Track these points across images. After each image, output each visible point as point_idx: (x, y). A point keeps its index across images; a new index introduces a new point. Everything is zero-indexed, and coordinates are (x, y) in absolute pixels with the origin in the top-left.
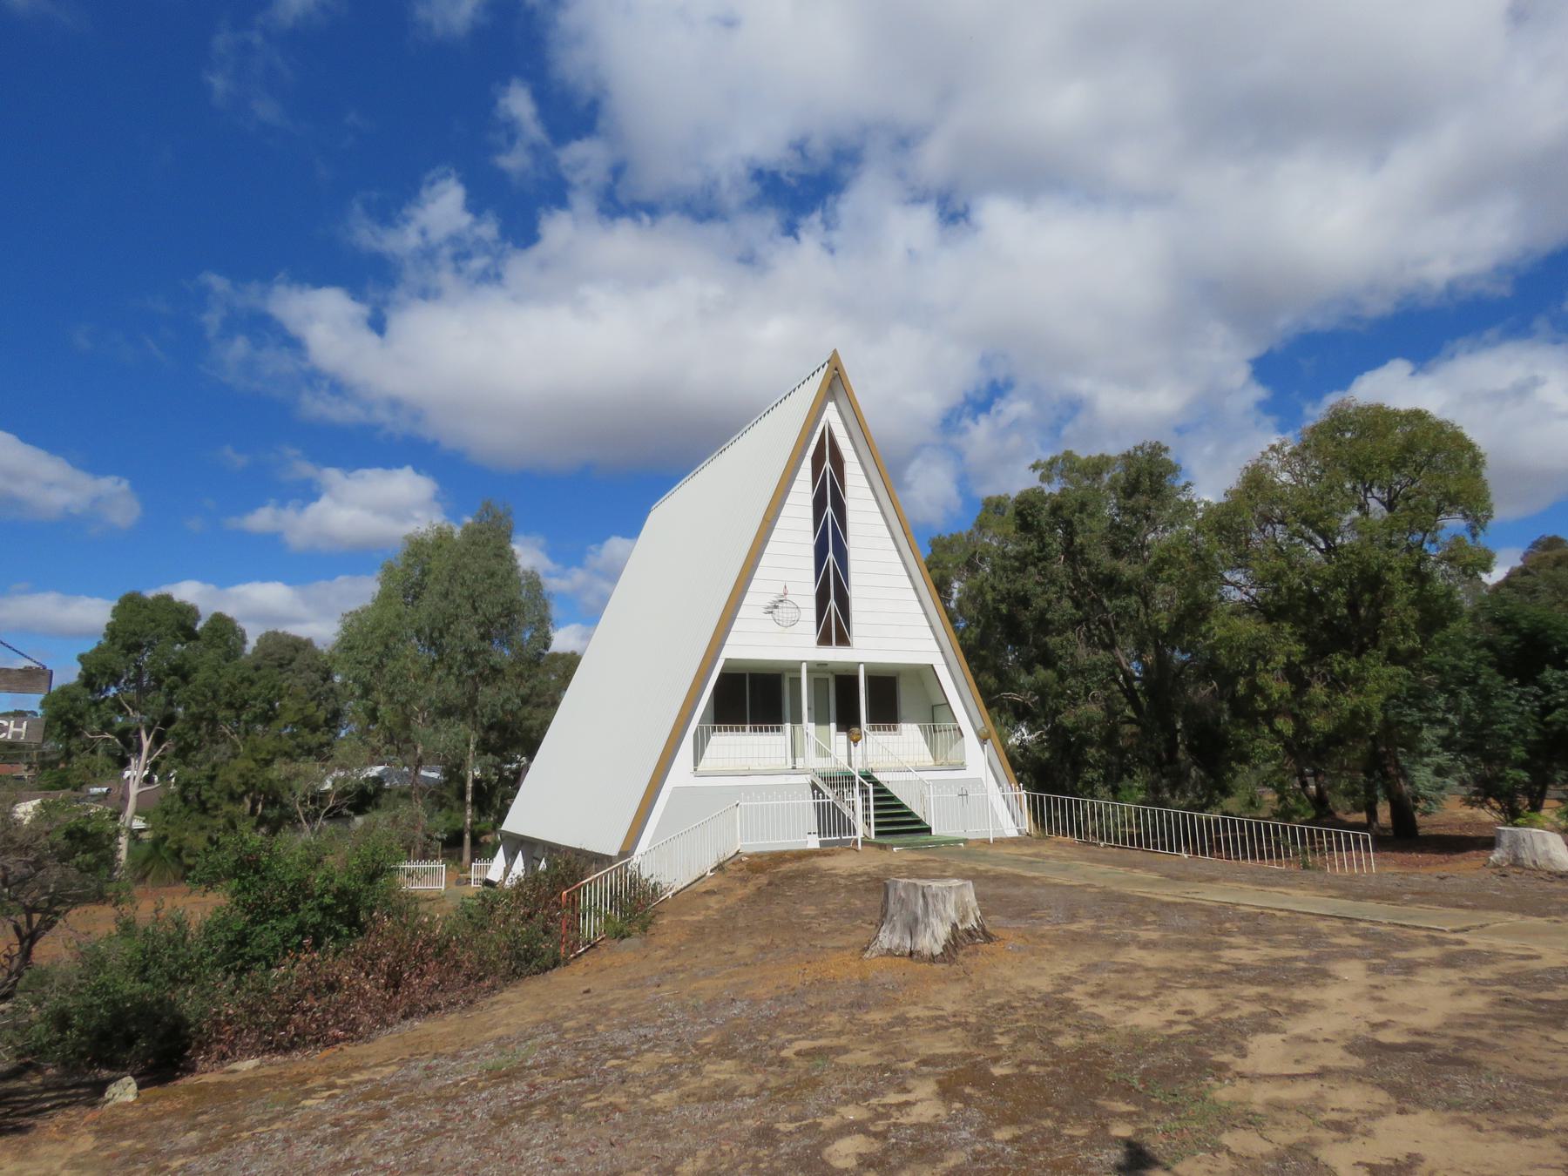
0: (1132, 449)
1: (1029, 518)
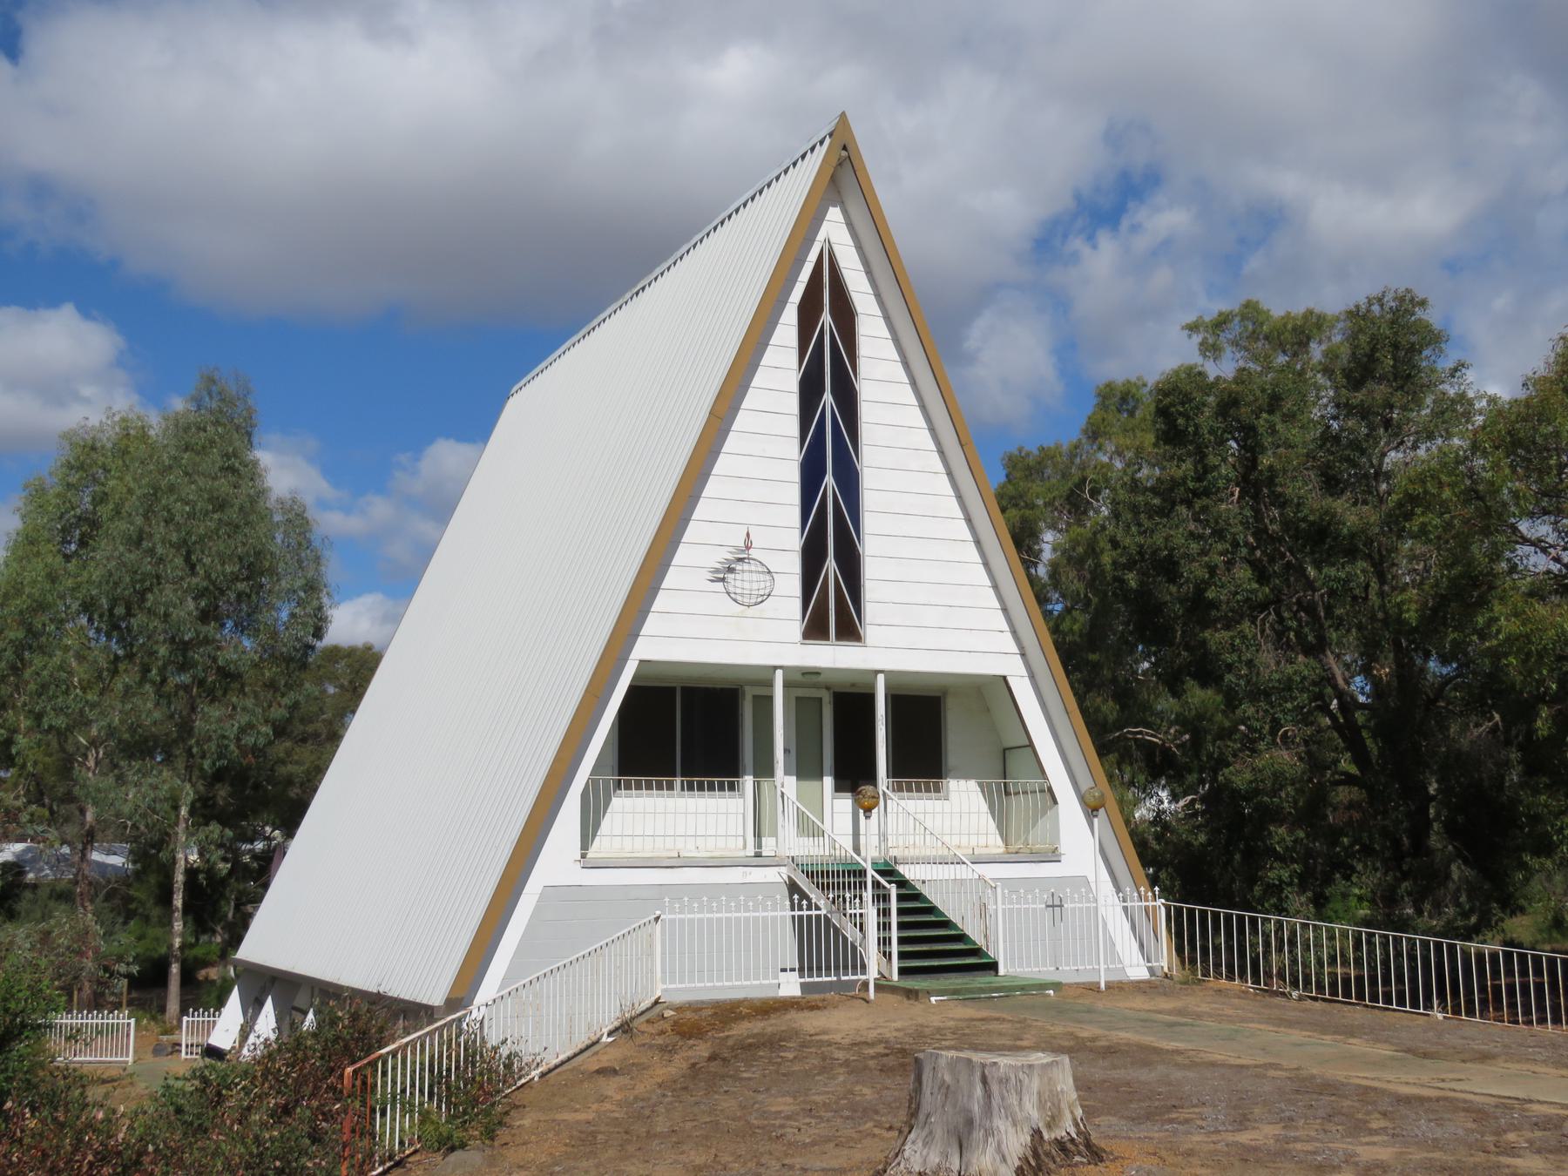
1: (1181, 421)
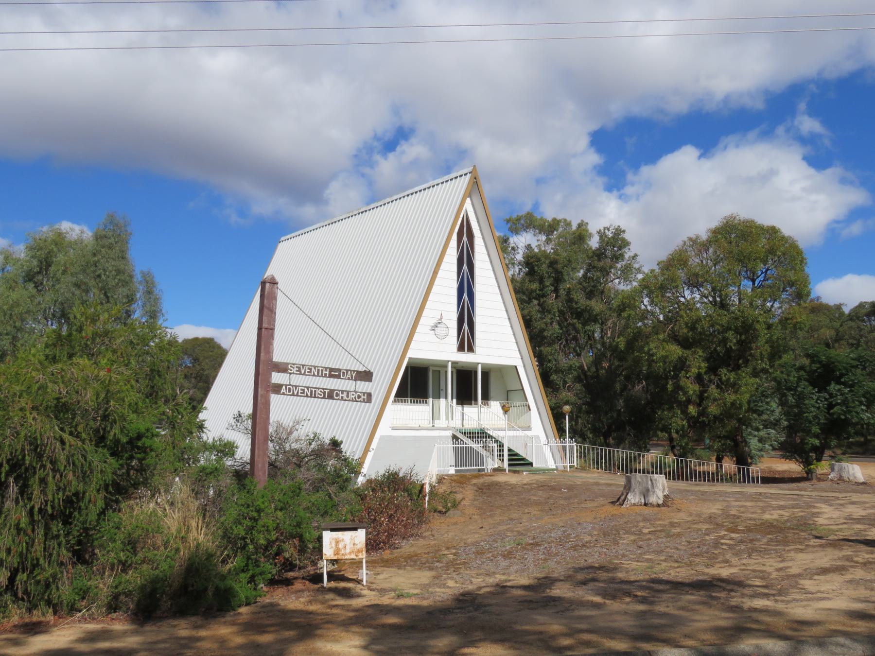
0: (602, 229)
1: (536, 268)
